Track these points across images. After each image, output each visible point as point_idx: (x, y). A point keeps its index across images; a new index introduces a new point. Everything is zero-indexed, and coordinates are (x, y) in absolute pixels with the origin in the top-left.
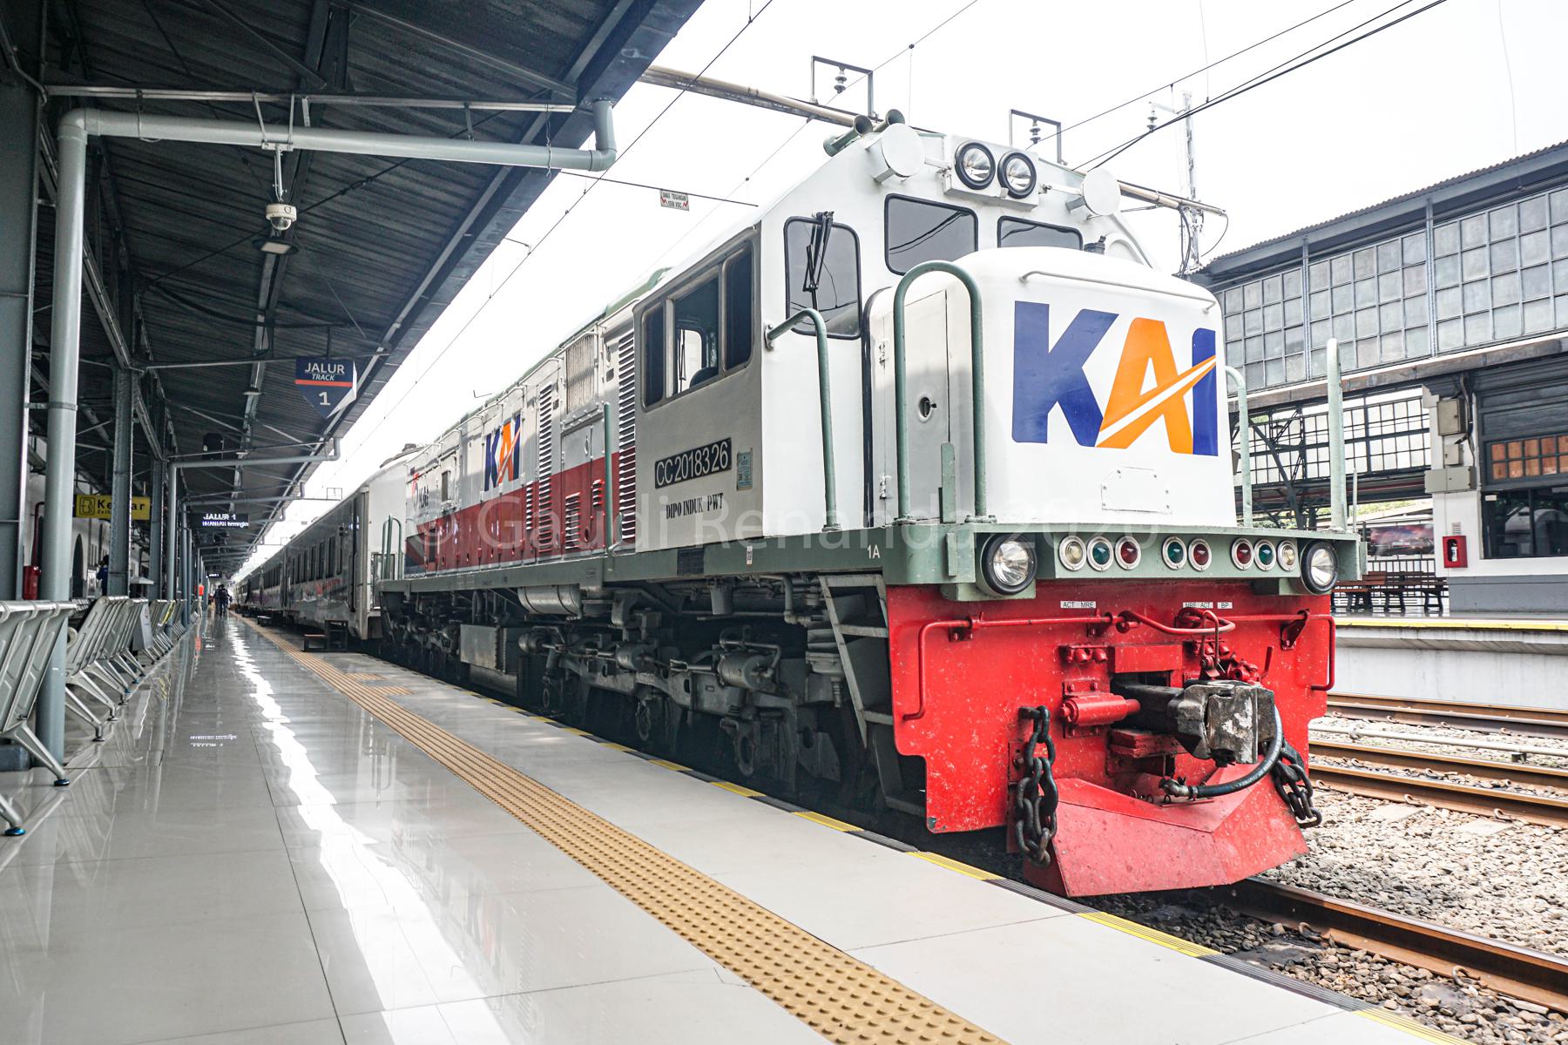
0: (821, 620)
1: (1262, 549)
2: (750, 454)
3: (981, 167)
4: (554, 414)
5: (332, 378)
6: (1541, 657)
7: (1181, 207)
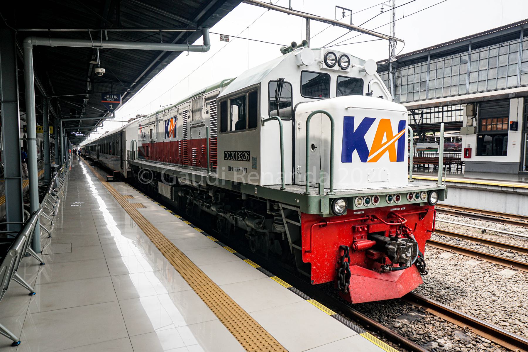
0: (279, 213)
1: (416, 194)
2: (256, 158)
3: (333, 60)
4: (189, 120)
5: (113, 100)
6: (492, 192)
7: (390, 39)
